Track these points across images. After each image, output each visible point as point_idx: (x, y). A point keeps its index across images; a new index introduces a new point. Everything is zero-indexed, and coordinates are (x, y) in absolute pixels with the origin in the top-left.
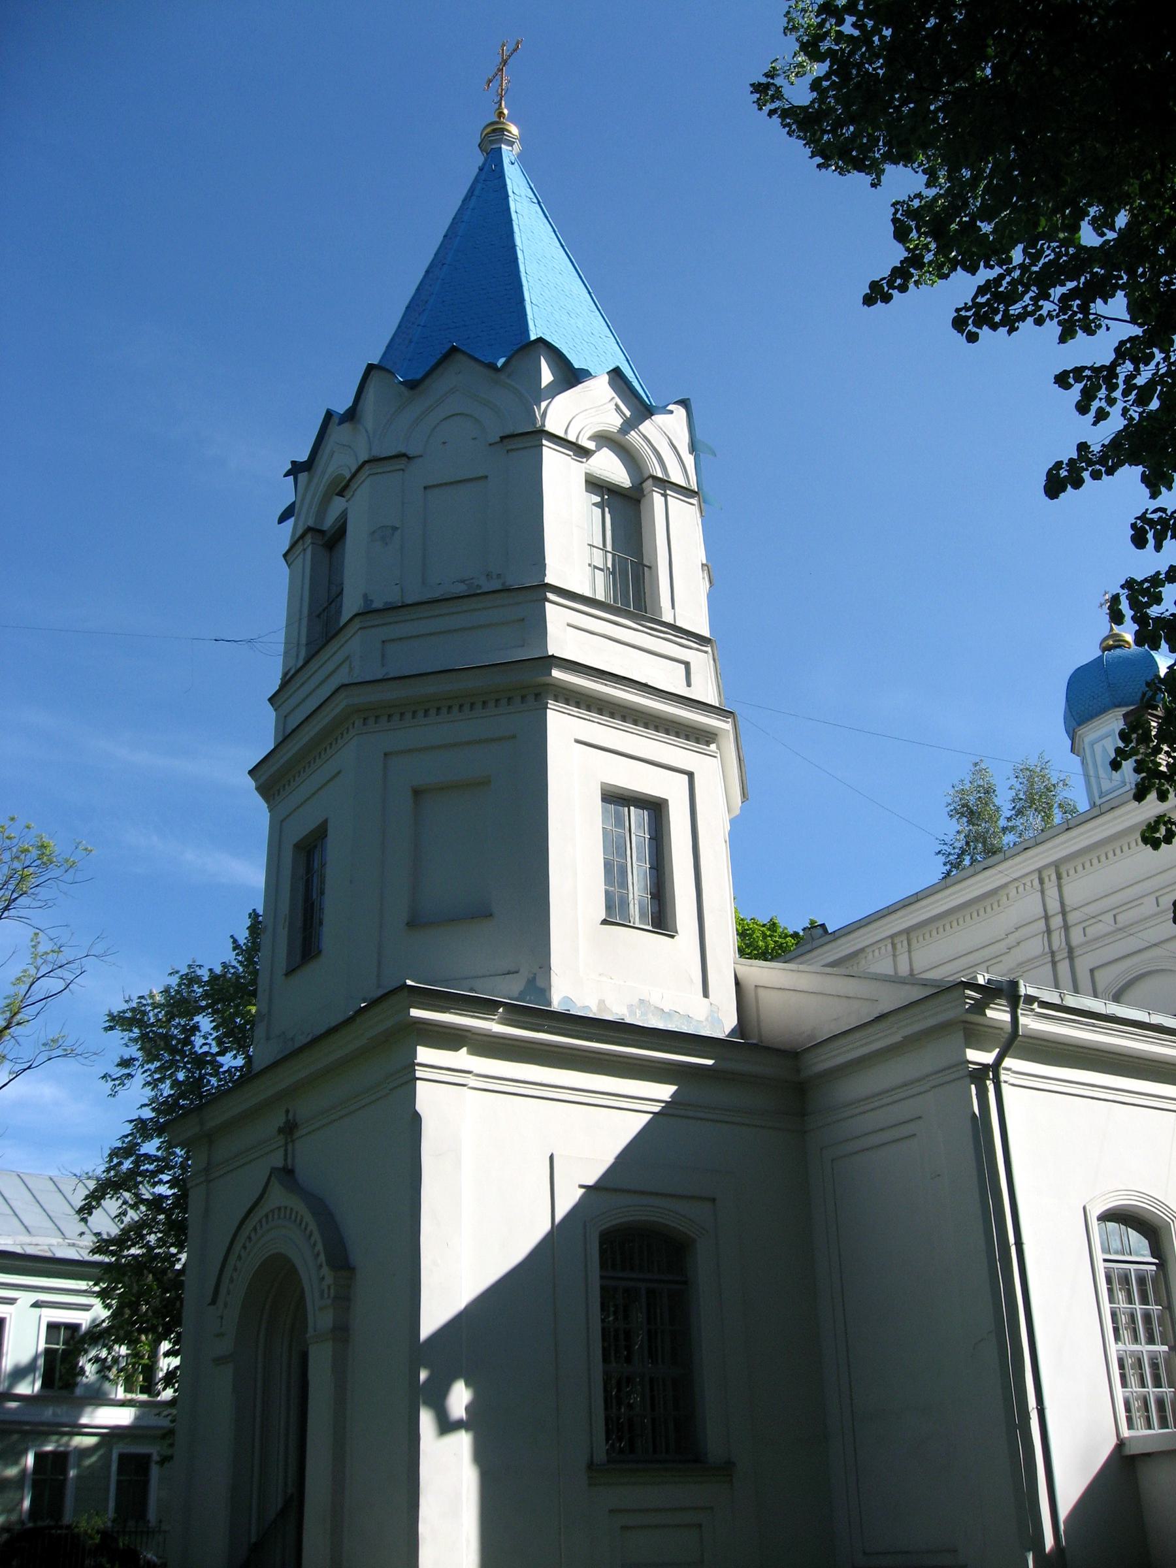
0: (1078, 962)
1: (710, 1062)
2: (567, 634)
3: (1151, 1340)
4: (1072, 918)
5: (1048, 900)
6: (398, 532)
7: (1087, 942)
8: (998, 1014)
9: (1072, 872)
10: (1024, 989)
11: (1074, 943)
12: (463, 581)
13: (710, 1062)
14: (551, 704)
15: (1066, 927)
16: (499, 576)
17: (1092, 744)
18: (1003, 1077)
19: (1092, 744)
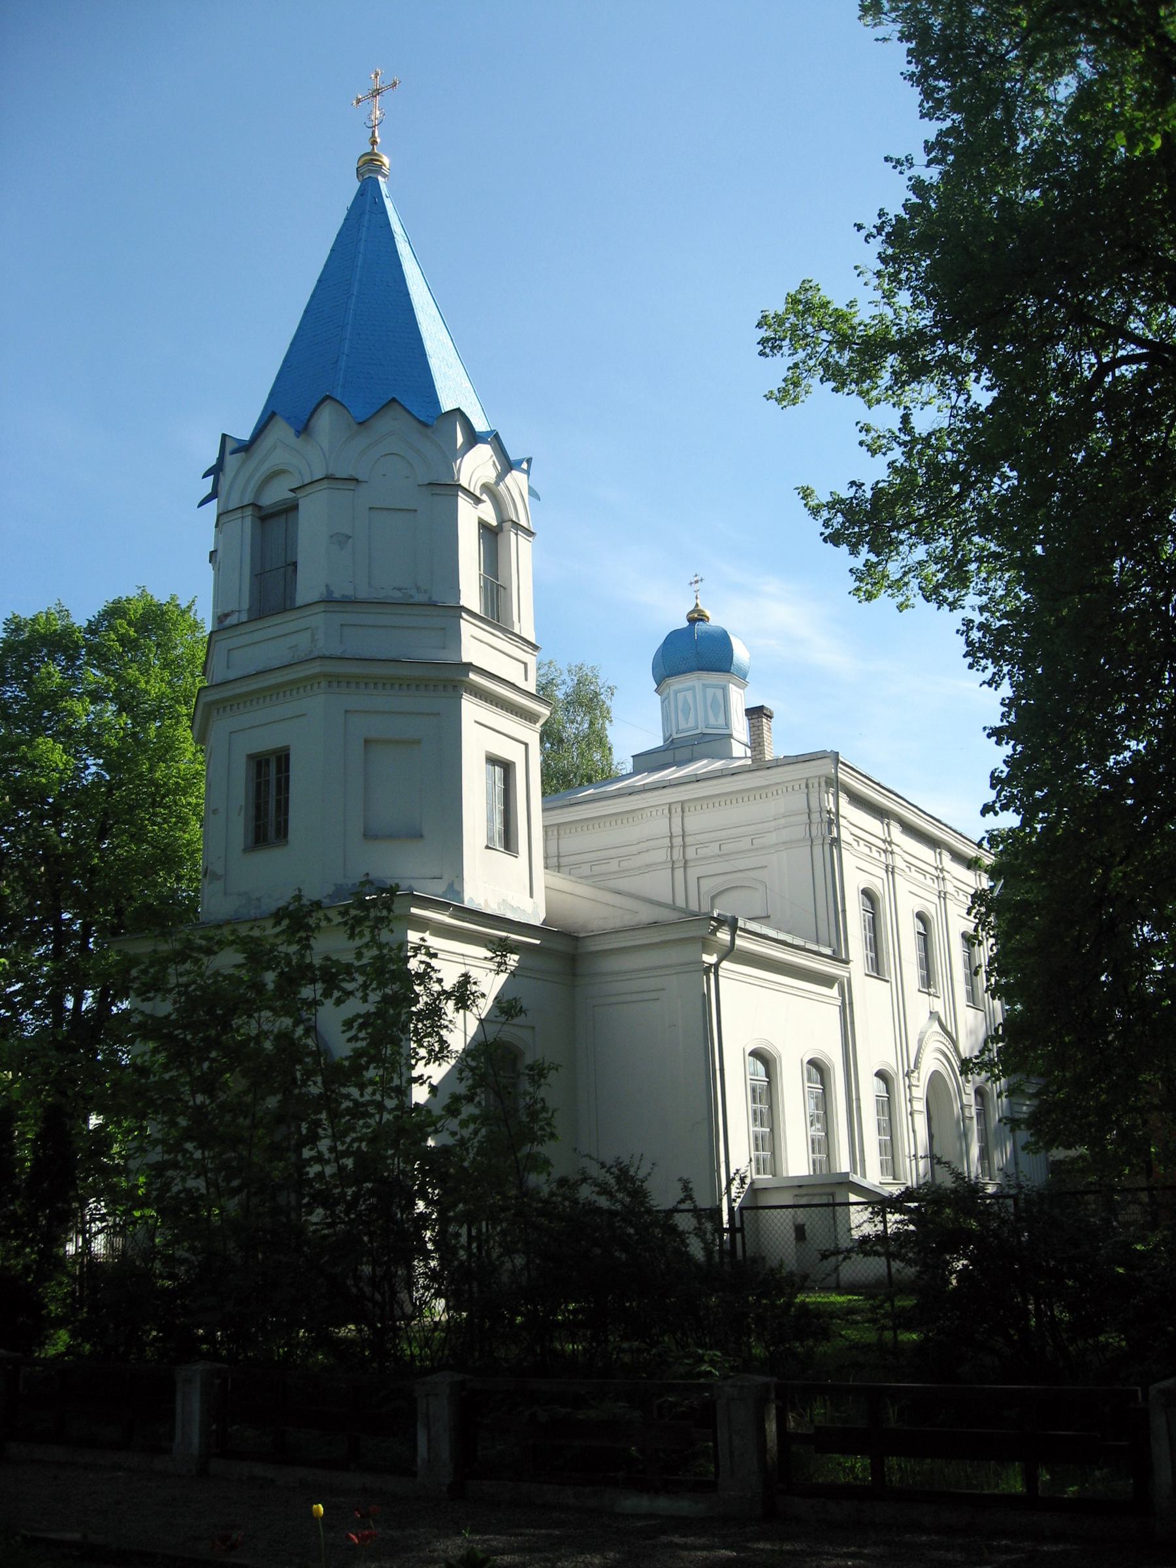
0: (689, 871)
1: (538, 942)
2: (476, 646)
3: (762, 1126)
4: (688, 840)
5: (673, 826)
6: (350, 541)
7: (697, 859)
8: (724, 936)
9: (692, 809)
10: (741, 924)
11: (688, 857)
12: (400, 589)
13: (538, 942)
14: (465, 696)
15: (684, 846)
16: (426, 591)
17: (676, 692)
18: (720, 973)
19: (676, 692)
